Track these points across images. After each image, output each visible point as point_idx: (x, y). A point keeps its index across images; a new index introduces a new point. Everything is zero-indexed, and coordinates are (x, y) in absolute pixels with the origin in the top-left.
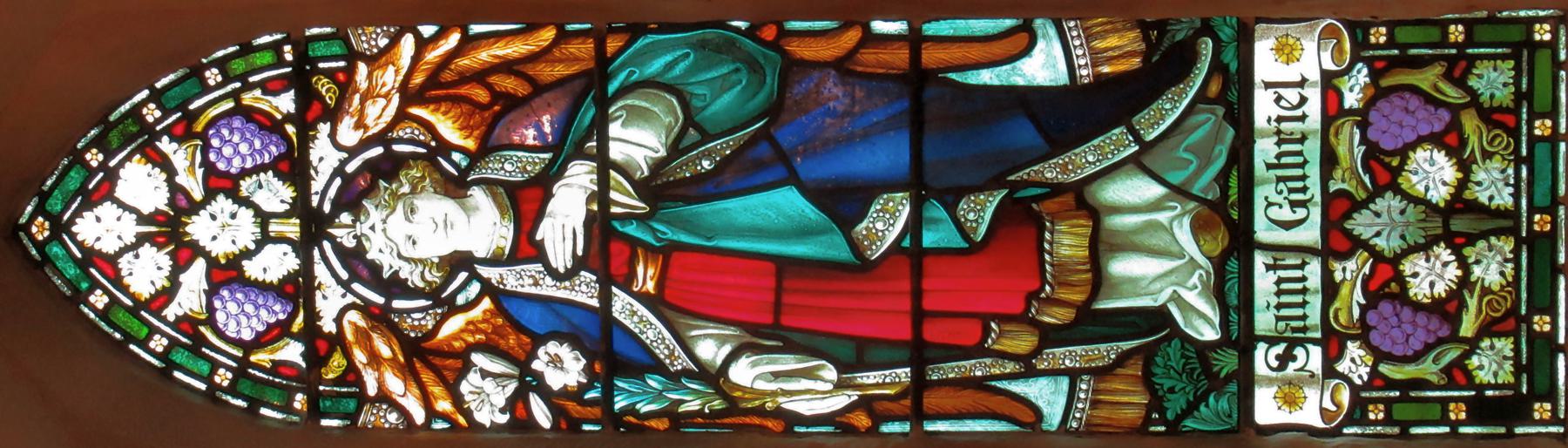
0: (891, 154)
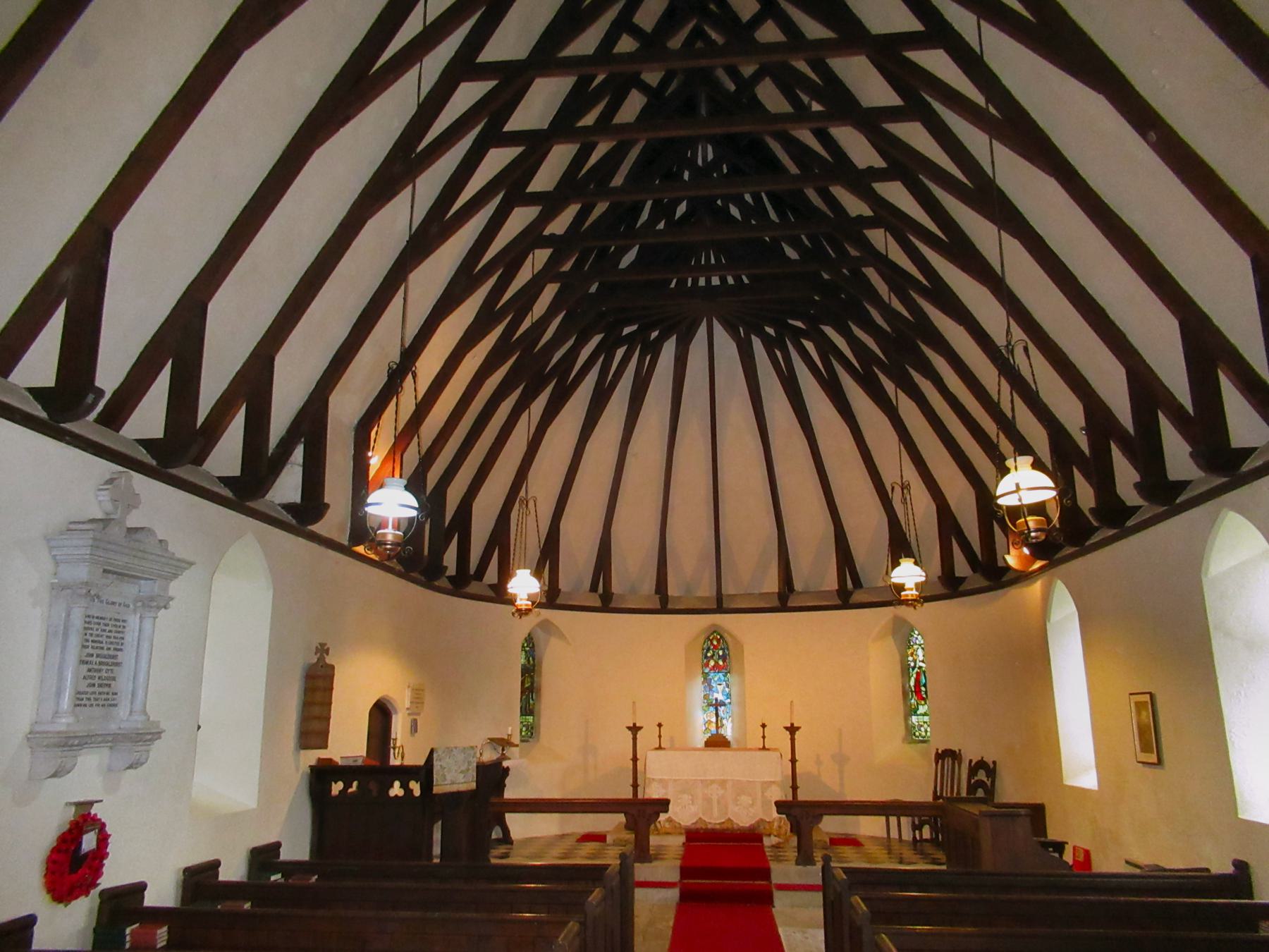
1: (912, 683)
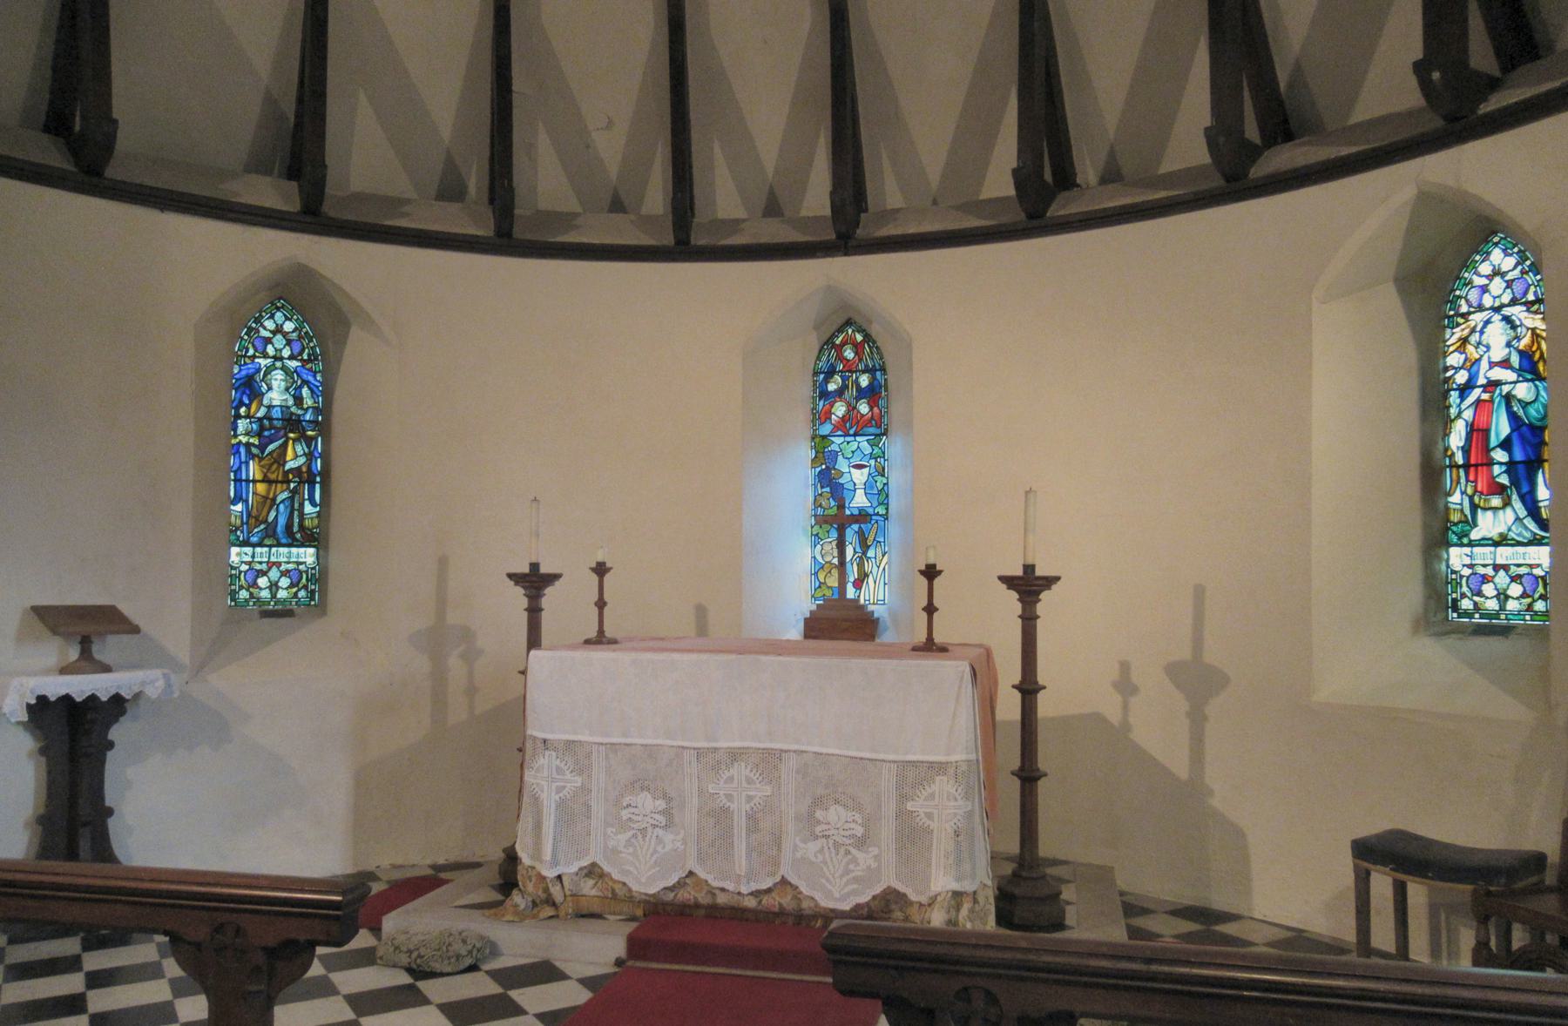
0: (1519, 455)
1: (1457, 439)
